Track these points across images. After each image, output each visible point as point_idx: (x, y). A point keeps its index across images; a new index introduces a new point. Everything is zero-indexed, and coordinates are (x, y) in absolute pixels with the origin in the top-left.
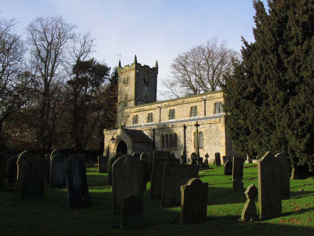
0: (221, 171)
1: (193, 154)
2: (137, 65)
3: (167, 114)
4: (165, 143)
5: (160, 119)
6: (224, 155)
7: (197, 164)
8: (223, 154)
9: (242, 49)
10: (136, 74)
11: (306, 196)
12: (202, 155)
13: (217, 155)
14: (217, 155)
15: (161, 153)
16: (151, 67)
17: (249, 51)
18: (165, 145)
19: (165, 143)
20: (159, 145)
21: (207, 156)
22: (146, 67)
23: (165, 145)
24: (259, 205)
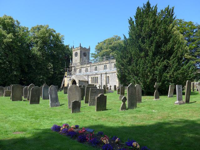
0: (117, 92)
1: (104, 86)
2: (81, 48)
3: (94, 68)
4: (93, 81)
5: (101, 83)
6: (118, 86)
7: (132, 84)
8: (117, 85)
9: (130, 19)
10: (81, 51)
11: (64, 81)
12: (109, 86)
13: (115, 86)
14: (115, 86)
15: (90, 85)
16: (87, 48)
17: (126, 41)
18: (93, 82)
19: (93, 81)
20: (90, 83)
21: (111, 87)
22: (85, 48)
23: (93, 82)
24: (127, 103)
